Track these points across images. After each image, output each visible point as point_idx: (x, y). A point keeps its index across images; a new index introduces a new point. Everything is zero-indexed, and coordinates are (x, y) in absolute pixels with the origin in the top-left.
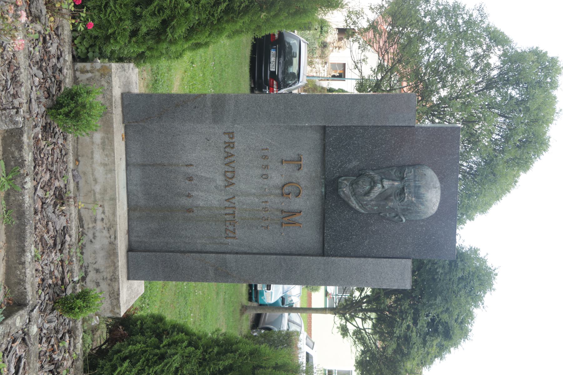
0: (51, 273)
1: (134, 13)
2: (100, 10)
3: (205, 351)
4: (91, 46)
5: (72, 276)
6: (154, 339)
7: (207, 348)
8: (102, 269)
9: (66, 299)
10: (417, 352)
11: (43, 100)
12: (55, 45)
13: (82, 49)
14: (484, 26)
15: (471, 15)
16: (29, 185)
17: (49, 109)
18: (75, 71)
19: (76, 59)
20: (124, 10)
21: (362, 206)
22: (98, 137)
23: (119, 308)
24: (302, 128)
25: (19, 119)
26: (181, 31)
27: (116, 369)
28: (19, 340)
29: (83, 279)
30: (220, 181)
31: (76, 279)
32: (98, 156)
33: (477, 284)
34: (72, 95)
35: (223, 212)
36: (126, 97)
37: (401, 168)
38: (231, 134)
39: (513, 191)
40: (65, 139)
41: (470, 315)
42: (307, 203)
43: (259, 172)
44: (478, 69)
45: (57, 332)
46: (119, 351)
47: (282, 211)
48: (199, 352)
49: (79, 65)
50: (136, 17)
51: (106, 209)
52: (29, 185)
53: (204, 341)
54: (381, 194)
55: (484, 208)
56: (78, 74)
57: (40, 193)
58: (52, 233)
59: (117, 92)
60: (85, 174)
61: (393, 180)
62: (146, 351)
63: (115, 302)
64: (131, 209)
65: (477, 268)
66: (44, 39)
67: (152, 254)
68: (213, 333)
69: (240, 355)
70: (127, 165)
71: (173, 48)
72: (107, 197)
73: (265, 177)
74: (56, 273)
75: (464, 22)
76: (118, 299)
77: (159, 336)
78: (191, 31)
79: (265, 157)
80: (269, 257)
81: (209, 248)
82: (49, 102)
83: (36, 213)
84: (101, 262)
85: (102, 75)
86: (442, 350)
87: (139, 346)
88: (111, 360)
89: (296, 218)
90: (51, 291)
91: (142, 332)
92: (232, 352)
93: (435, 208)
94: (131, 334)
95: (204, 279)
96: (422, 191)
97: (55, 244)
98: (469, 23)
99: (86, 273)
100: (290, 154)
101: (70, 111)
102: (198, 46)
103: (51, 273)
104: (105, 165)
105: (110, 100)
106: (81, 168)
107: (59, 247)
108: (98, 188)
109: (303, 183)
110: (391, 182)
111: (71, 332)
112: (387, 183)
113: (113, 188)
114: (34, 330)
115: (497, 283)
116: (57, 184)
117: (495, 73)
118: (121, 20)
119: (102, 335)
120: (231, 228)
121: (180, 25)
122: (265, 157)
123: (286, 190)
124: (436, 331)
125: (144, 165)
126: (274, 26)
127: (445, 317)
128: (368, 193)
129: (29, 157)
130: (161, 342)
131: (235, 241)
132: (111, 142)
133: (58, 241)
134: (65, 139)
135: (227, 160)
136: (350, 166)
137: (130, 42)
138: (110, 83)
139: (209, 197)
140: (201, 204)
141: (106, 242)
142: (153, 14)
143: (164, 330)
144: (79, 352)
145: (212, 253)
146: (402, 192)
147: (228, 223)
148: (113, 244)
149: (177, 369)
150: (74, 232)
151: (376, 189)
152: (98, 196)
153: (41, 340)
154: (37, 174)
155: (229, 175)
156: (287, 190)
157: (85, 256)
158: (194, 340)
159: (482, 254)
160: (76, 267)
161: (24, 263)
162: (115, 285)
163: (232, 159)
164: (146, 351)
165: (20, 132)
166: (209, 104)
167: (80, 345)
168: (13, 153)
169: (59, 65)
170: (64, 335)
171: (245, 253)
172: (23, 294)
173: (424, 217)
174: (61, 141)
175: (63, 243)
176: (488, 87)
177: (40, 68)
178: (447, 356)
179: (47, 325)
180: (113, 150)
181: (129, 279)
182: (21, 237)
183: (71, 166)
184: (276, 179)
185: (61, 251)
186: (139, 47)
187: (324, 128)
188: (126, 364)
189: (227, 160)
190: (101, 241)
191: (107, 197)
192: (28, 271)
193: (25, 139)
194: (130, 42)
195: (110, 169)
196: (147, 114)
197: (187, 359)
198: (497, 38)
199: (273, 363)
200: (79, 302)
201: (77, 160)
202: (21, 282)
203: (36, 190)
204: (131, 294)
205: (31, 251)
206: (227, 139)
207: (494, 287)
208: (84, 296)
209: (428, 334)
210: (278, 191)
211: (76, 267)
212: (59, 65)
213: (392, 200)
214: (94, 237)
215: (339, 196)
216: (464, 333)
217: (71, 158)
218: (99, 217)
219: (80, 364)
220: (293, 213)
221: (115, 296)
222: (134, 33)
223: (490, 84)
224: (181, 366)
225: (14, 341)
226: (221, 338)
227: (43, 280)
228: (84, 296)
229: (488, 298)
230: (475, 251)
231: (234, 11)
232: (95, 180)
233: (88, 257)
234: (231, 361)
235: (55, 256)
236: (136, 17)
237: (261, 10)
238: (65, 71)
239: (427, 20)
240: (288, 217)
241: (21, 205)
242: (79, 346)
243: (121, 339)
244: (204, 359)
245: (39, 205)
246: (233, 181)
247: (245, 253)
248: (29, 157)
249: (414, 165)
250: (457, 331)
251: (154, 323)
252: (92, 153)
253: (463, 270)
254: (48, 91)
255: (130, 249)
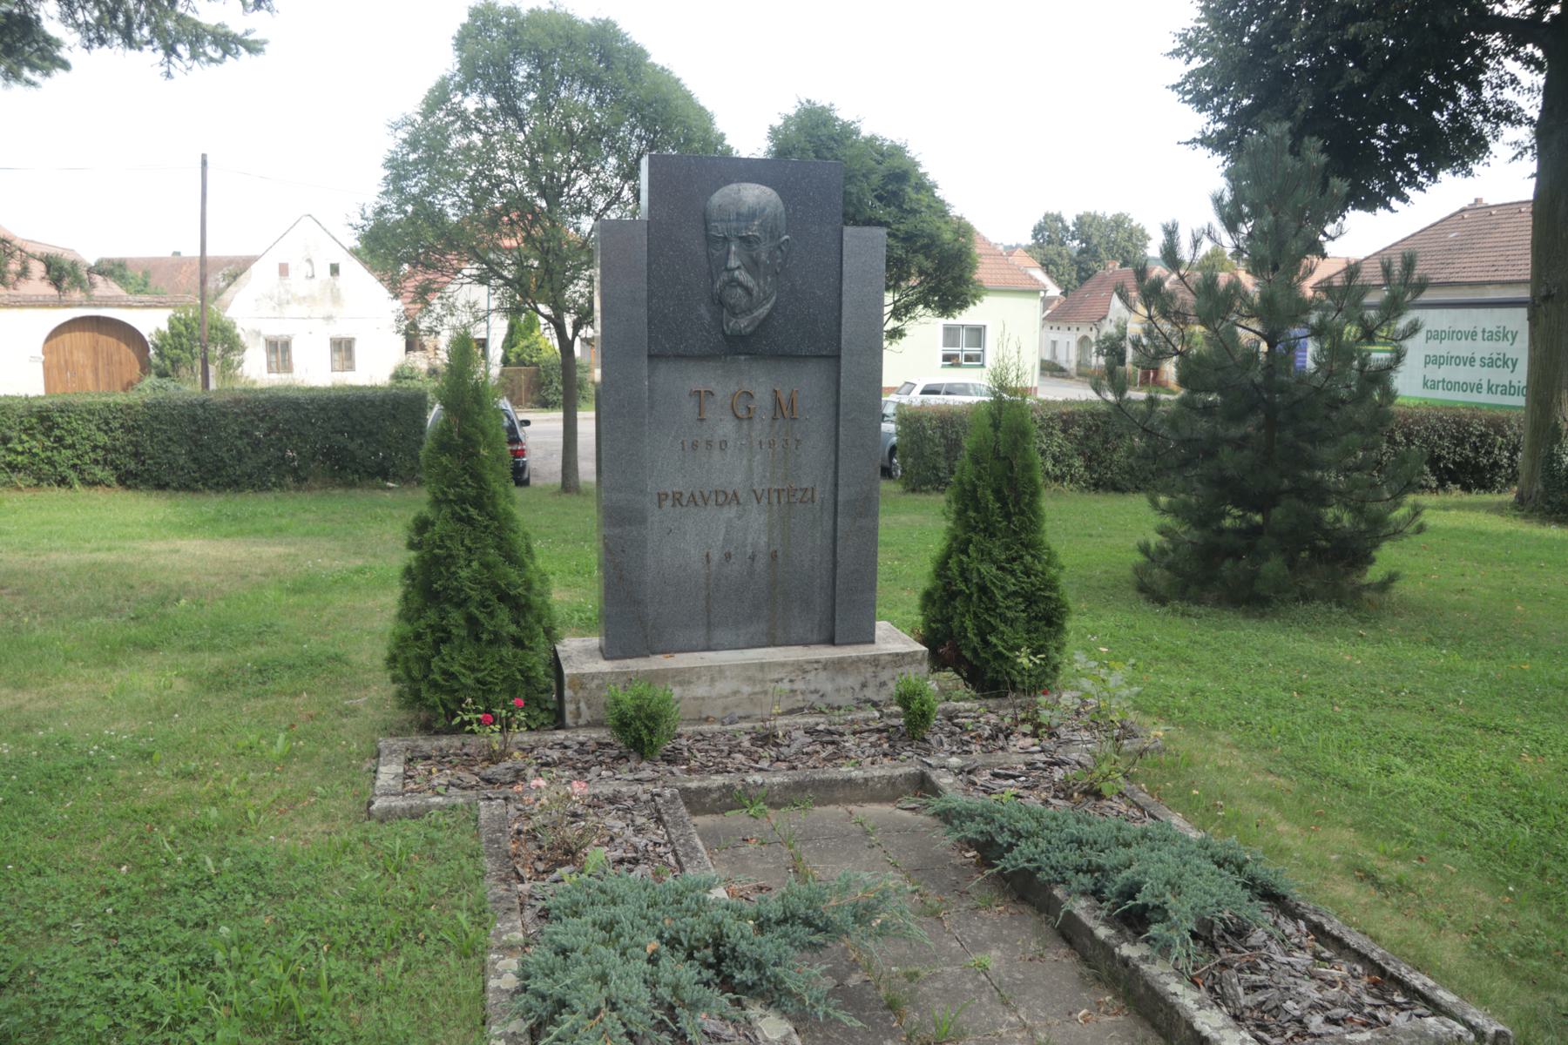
0: (873, 745)
1: (490, 643)
2: (490, 691)
3: (974, 529)
4: (538, 706)
5: (874, 719)
6: (958, 603)
7: (969, 527)
8: (861, 679)
9: (908, 723)
10: (928, 223)
11: (632, 764)
12: (548, 752)
13: (542, 717)
14: (419, 119)
15: (405, 141)
16: (758, 778)
17: (643, 757)
18: (578, 726)
19: (559, 724)
20: (487, 657)
21: (767, 299)
22: (677, 692)
23: (915, 653)
24: (650, 390)
25: (667, 793)
26: (513, 574)
27: (999, 653)
28: (972, 777)
29: (875, 705)
30: (730, 512)
31: (877, 714)
32: (700, 690)
33: (824, 131)
34: (622, 724)
35: (775, 507)
36: (607, 653)
37: (710, 240)
38: (661, 497)
39: (677, 74)
40: (680, 736)
41: (871, 140)
42: (761, 383)
43: (716, 453)
44: (483, 128)
45: (953, 733)
46: (975, 650)
47: (774, 419)
48: (976, 538)
49: (569, 720)
50: (496, 640)
51: (776, 676)
52: (758, 778)
53: (959, 532)
54: (748, 271)
55: (704, 117)
56: (581, 722)
57: (764, 764)
58: (818, 748)
59: (605, 666)
60: (726, 708)
61: (728, 252)
62: (975, 613)
63: (908, 659)
64: (773, 643)
65: (798, 129)
66: (543, 765)
67: (838, 611)
68: (948, 519)
69: (979, 478)
70: (709, 649)
71: (537, 586)
72: (759, 676)
73: (723, 444)
74: (873, 739)
75: (414, 151)
76: (904, 655)
77: (953, 595)
78: (512, 559)
79: (694, 446)
80: (842, 437)
81: (828, 526)
82: (633, 757)
83: (794, 768)
84: (852, 681)
85: (582, 687)
86: (924, 187)
87: (968, 624)
88: (988, 662)
89: (784, 397)
90: (899, 745)
91: (947, 620)
92: (975, 491)
93: (768, 190)
94: (950, 635)
95: (873, 532)
96: (744, 210)
97: (833, 743)
98: (413, 144)
99: (867, 701)
100: (690, 407)
101: (647, 727)
102: (529, 550)
103: (873, 745)
104: (713, 680)
105: (619, 675)
106: (718, 714)
107: (836, 737)
108: (746, 689)
109: (733, 387)
110: (732, 256)
111: (951, 717)
112: (733, 262)
113: (746, 667)
114: (955, 761)
115: (821, 100)
116: (746, 744)
117: (491, 102)
118: (501, 662)
119: (948, 677)
120: (799, 495)
121: (506, 575)
122: (694, 446)
123: (742, 413)
124: (894, 194)
125: (709, 625)
126: (497, 435)
127: (876, 179)
128: (748, 291)
129: (718, 780)
130: (961, 592)
131: (818, 490)
132: (679, 671)
133: (828, 738)
134: (680, 736)
135: (700, 501)
136: (707, 317)
137: (531, 649)
138: (593, 676)
139: (754, 528)
140: (764, 539)
141: (823, 675)
142: (491, 615)
143: (944, 589)
144: (976, 705)
145: (835, 523)
146: (746, 241)
147: (793, 500)
148: (826, 665)
149: (1000, 568)
150: (811, 720)
151: (741, 278)
152: (758, 688)
153: (966, 752)
154: (739, 770)
155: (721, 499)
156: (742, 412)
157: (843, 704)
158: (958, 545)
159: (778, 122)
160: (861, 715)
161: (866, 780)
162: (883, 660)
163: (697, 494)
164: (975, 613)
165: (685, 792)
166: (618, 531)
167: (968, 705)
168: (714, 801)
169: (576, 747)
170: (956, 725)
171: (836, 473)
172: (908, 778)
173: (781, 208)
174: (684, 741)
175: (830, 733)
176: (514, 112)
177: (587, 770)
178: (931, 177)
179: (946, 747)
180: (691, 669)
181: (873, 642)
182: (831, 785)
183: (716, 727)
184: (726, 428)
185: (842, 735)
186: (538, 635)
187: (650, 357)
188: (993, 640)
189: (700, 501)
190: (822, 682)
191: (759, 676)
192: (876, 774)
193: (693, 785)
194: (531, 649)
195: (718, 673)
196: (630, 622)
197: (986, 555)
198: (438, 98)
199: (990, 430)
200: (915, 705)
201: (706, 720)
202: (891, 782)
203: (761, 770)
204: (895, 637)
205: (847, 771)
206: (669, 503)
207: (826, 104)
208: (904, 700)
209: (900, 207)
210: (745, 425)
211: (861, 715)
212: (576, 747)
213: (759, 255)
214: (816, 691)
215: (753, 334)
216: (897, 151)
217: (705, 728)
218: (786, 686)
219: (992, 703)
220: (777, 402)
221: (899, 659)
222: (518, 643)
223: (509, 109)
224: (994, 562)
225: (974, 784)
226: (954, 506)
227: (885, 755)
228: (904, 700)
229: (844, 114)
230: (774, 132)
231: (479, 497)
232: (735, 693)
233: (845, 699)
234: (988, 492)
235: (850, 742)
236: (496, 640)
237: (477, 454)
238: (581, 738)
239: (409, 208)
240: (783, 409)
241: (787, 787)
242: (968, 705)
243: (956, 649)
244: (985, 530)
245: (783, 765)
246: (730, 493)
247: (836, 473)
248: (718, 780)
249: (706, 222)
250: (895, 162)
251: (934, 604)
252: (696, 699)
253: (803, 150)
254: (617, 759)
255: (831, 641)
